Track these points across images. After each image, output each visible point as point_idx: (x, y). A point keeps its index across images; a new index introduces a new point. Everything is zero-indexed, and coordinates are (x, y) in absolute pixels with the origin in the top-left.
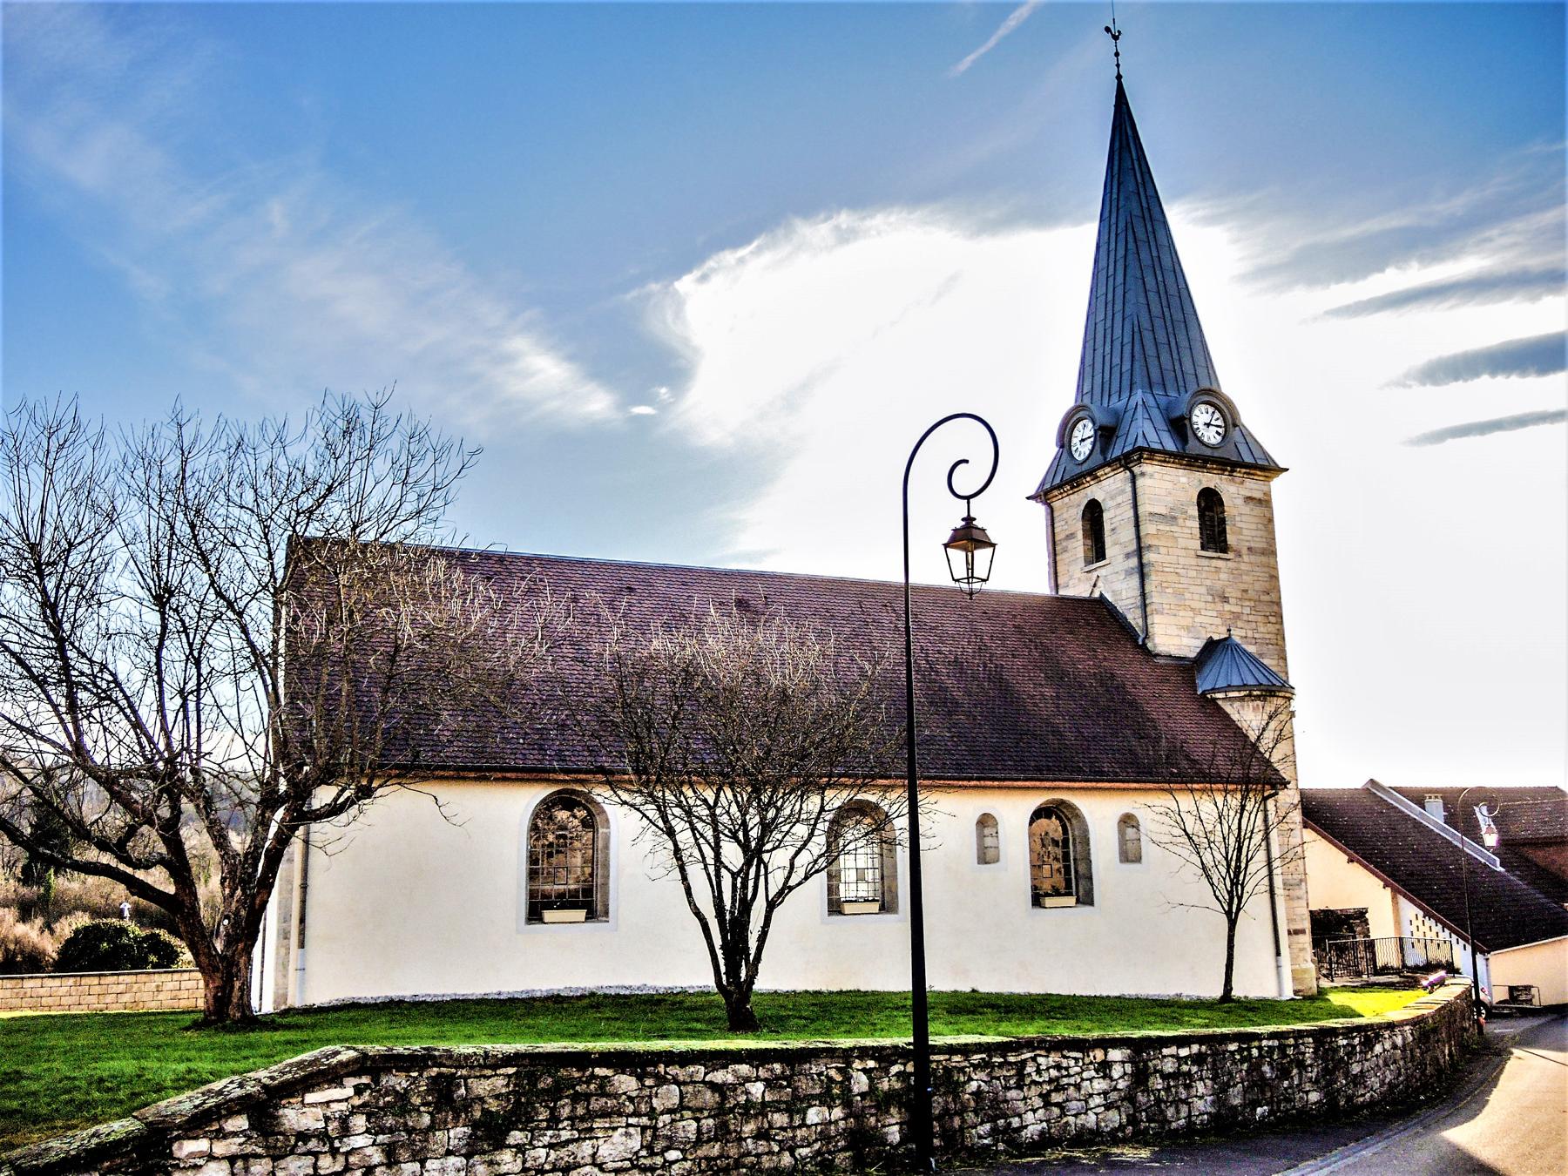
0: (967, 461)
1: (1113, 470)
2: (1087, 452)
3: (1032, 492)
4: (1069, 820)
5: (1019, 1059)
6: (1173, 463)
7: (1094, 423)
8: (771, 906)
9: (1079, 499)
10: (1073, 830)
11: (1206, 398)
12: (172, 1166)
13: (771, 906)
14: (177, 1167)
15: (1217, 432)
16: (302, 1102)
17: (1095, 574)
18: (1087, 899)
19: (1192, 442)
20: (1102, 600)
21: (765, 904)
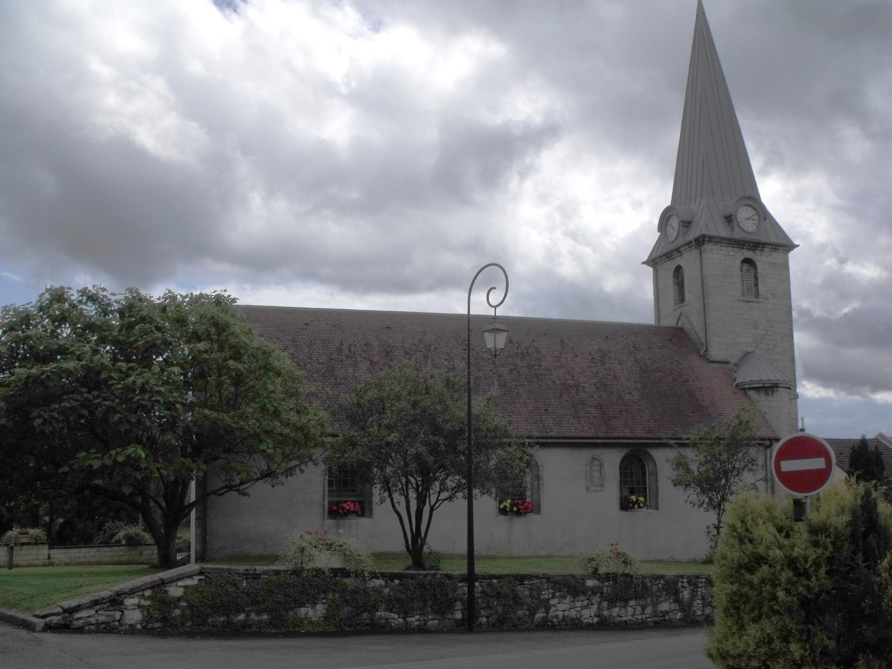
0: (495, 288)
1: (689, 247)
2: (675, 236)
3: (645, 259)
4: (645, 460)
5: (531, 582)
6: (725, 243)
7: (678, 218)
8: (432, 509)
9: (671, 265)
10: (649, 467)
11: (747, 202)
12: (124, 608)
13: (432, 509)
14: (126, 608)
15: (753, 223)
16: (176, 585)
17: (679, 311)
18: (657, 509)
19: (737, 229)
20: (681, 330)
21: (429, 509)
